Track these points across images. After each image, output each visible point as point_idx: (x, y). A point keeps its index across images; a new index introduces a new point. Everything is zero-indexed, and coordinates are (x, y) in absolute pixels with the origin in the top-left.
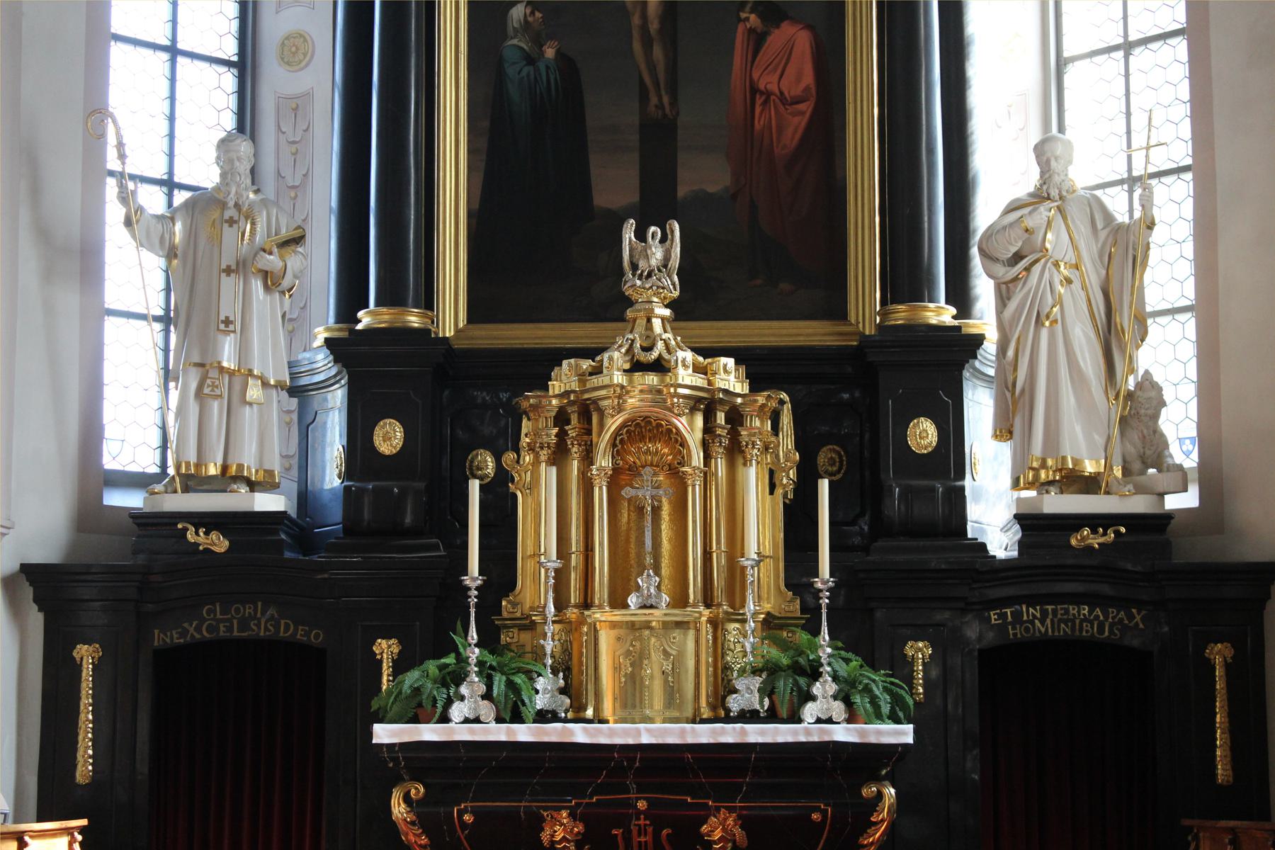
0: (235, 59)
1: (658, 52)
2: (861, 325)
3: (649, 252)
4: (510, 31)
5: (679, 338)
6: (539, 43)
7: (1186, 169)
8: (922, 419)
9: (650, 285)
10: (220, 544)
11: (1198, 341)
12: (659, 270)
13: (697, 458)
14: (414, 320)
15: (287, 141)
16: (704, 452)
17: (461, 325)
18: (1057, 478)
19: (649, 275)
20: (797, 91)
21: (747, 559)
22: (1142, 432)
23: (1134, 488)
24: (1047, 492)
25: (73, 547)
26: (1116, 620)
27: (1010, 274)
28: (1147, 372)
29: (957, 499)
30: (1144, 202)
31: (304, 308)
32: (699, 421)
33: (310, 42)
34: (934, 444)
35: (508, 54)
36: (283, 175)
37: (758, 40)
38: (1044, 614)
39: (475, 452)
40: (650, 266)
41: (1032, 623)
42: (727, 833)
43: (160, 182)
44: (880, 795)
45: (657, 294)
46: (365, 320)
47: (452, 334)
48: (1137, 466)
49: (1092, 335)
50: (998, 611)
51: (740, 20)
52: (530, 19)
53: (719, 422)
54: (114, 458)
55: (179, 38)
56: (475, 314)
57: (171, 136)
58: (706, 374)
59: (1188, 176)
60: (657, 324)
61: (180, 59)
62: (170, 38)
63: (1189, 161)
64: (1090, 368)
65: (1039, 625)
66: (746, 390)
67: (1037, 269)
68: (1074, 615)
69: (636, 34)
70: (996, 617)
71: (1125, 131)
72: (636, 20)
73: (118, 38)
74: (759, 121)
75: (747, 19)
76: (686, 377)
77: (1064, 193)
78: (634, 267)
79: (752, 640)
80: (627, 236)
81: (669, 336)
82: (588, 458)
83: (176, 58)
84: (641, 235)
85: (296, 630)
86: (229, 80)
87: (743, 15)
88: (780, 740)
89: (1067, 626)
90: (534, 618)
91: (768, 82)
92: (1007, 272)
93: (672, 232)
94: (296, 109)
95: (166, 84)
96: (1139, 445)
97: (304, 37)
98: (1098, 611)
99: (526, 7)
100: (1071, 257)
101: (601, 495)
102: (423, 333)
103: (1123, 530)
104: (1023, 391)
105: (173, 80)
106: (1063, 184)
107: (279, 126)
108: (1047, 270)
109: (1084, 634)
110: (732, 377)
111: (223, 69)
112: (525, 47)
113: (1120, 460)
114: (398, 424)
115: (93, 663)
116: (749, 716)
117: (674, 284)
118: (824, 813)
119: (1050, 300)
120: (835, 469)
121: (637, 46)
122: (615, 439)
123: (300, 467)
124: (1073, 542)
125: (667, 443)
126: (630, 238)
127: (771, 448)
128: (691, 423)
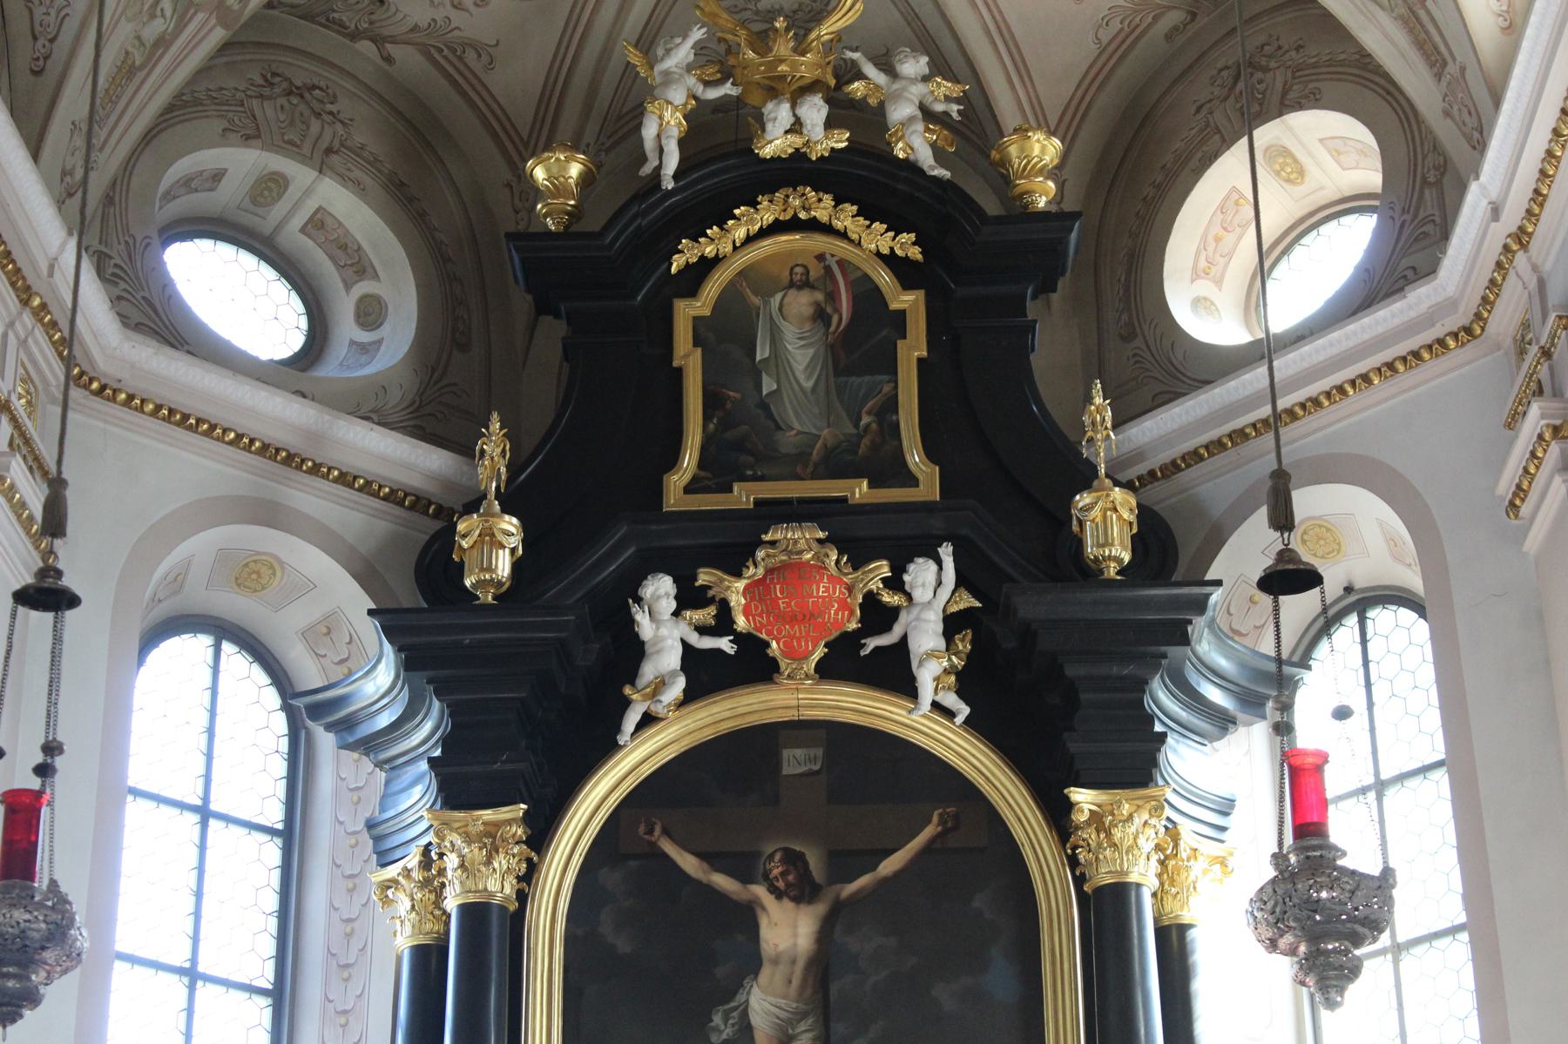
0: (280, 826)
11: (1477, 990)
15: (344, 876)
43: (180, 971)
55: (212, 798)
57: (197, 915)
59: (1464, 936)
61: (212, 822)
62: (201, 795)
63: (1442, 756)
71: (1361, 663)
73: (136, 793)
83: (208, 821)
86: (272, 852)
95: (194, 853)
105: (202, 847)
111: (265, 838)
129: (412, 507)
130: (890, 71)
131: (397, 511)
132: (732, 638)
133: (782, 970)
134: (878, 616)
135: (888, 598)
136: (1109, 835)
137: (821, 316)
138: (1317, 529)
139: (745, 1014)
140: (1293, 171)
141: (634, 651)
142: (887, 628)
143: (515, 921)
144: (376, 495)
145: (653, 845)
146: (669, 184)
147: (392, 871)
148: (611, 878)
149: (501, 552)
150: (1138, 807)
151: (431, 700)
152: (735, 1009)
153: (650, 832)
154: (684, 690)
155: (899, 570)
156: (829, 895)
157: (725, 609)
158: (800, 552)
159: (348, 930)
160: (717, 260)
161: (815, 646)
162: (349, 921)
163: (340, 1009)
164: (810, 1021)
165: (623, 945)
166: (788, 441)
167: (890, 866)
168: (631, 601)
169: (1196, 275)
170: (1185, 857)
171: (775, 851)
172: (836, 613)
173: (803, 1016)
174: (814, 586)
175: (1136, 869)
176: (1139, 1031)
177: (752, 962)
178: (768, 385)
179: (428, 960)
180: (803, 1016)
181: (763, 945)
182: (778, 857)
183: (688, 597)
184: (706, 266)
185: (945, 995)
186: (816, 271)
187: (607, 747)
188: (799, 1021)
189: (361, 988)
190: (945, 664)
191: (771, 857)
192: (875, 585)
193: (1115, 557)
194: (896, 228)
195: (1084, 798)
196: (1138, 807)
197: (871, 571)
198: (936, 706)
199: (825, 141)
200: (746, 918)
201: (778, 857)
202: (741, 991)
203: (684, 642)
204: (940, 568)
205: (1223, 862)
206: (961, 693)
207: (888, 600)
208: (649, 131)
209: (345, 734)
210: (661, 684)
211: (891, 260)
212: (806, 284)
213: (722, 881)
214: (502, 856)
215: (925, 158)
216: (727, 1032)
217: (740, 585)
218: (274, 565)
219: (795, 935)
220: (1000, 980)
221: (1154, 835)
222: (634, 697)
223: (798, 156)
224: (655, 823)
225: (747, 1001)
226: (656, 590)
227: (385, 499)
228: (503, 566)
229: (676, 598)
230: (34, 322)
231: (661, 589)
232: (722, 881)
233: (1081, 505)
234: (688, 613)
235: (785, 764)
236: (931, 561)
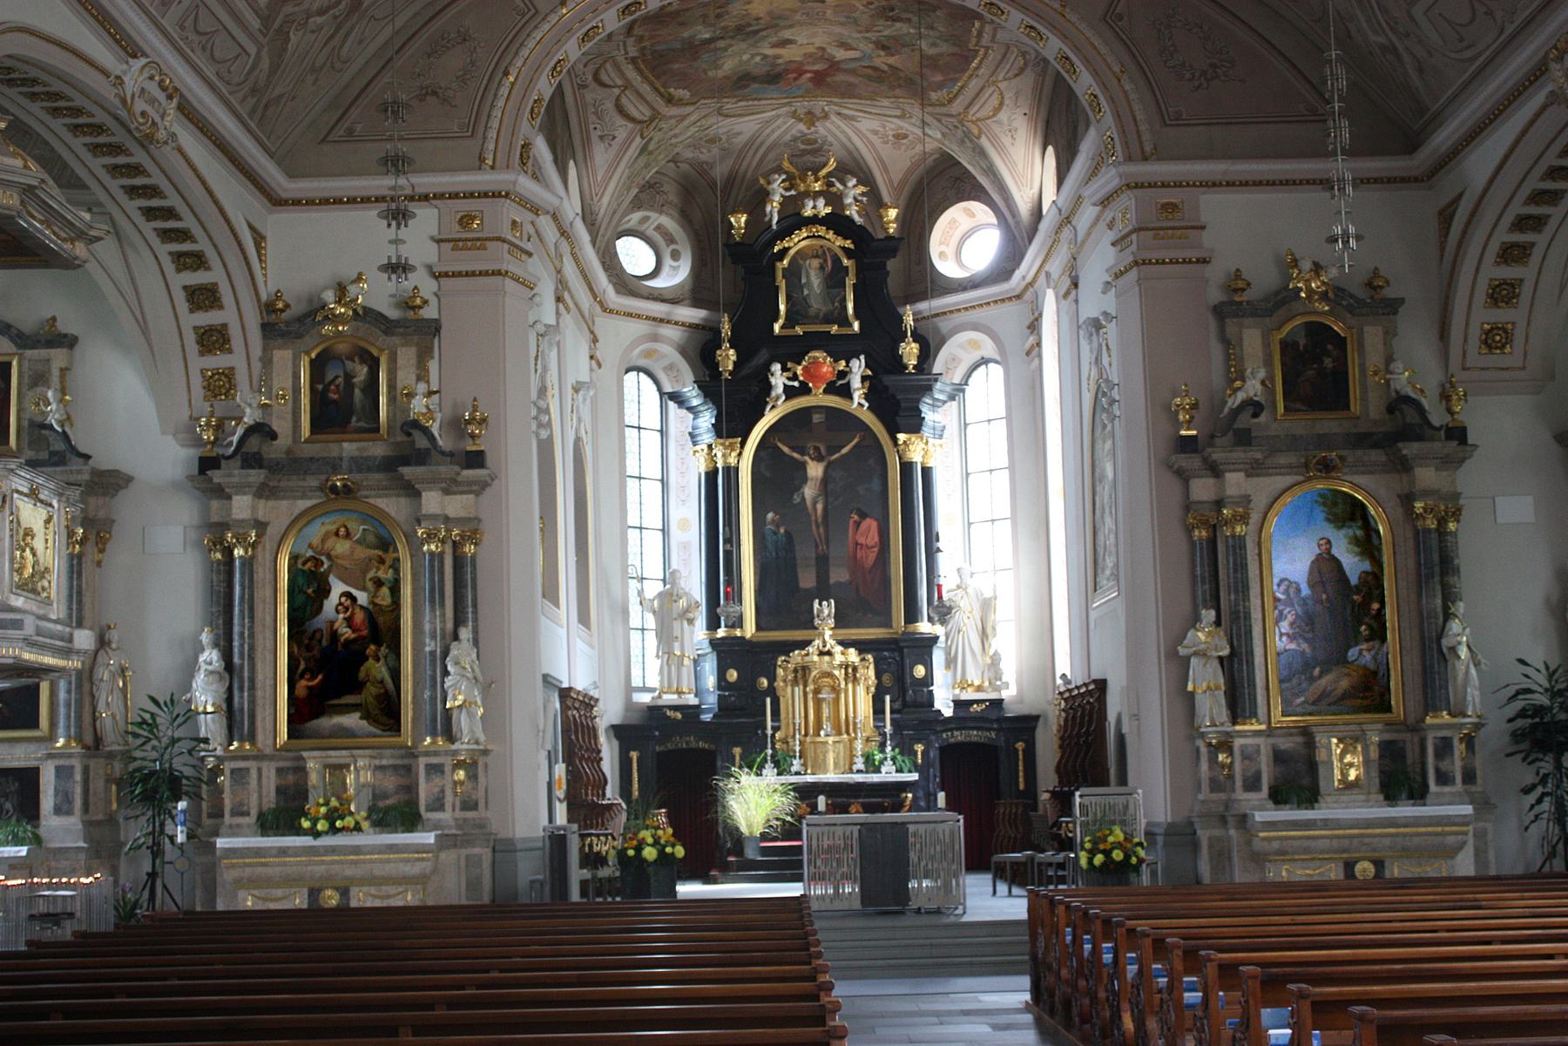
1: (821, 530)
6: (778, 527)
10: (679, 716)
13: (843, 686)
14: (738, 633)
20: (872, 544)
25: (625, 717)
28: (996, 653)
36: (355, 276)
37: (858, 524)
54: (636, 682)
56: (759, 627)
76: (839, 659)
82: (805, 686)
84: (820, 604)
88: (397, 902)
91: (861, 540)
101: (810, 696)
116: (859, 771)
121: (814, 527)
130: (844, 184)
134: (842, 374)
137: (822, 268)
140: (972, 215)
141: (769, 387)
142: (844, 378)
146: (774, 227)
147: (698, 448)
148: (763, 454)
160: (789, 248)
165: (768, 475)
166: (812, 312)
167: (845, 451)
169: (941, 243)
177: (805, 479)
178: (806, 292)
183: (784, 369)
184: (786, 250)
185: (861, 490)
186: (820, 252)
194: (846, 238)
195: (901, 437)
199: (824, 210)
200: (803, 465)
206: (866, 399)
208: (768, 209)
210: (778, 398)
211: (843, 248)
212: (817, 256)
213: (796, 455)
215: (857, 218)
217: (800, 368)
218: (655, 351)
220: (876, 485)
223: (815, 216)
230: (518, 189)
231: (776, 367)
232: (796, 455)
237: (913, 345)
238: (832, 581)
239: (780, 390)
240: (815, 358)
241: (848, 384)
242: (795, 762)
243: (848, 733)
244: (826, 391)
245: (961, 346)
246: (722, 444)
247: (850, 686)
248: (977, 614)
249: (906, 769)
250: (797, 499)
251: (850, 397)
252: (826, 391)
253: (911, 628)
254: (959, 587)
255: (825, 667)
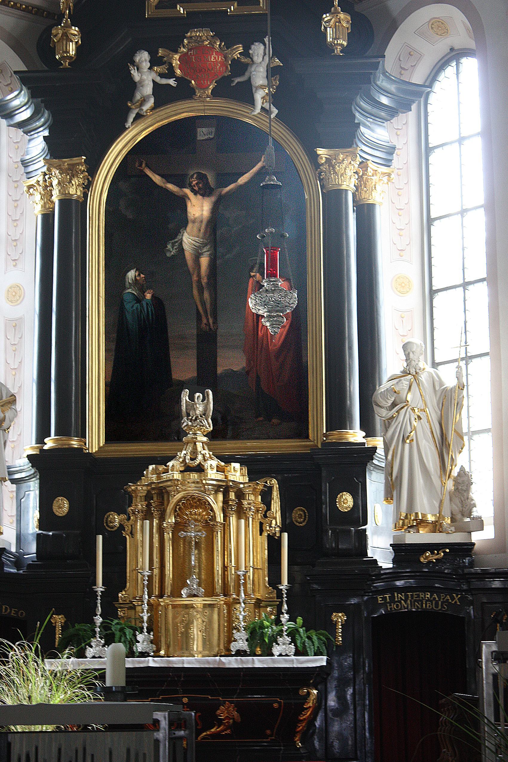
1: (206, 295)
2: (316, 442)
3: (195, 406)
4: (127, 285)
5: (211, 453)
6: (143, 291)
7: (487, 354)
8: (345, 493)
9: (196, 425)
12: (201, 416)
13: (220, 518)
14: (75, 443)
16: (224, 514)
17: (101, 445)
18: (415, 524)
19: (196, 419)
21: (240, 571)
22: (461, 498)
23: (455, 529)
24: (409, 532)
26: (445, 600)
27: (389, 414)
29: (362, 537)
30: (458, 376)
31: (20, 435)
32: (220, 497)
33: (22, 289)
34: (351, 506)
35: (126, 297)
38: (407, 597)
39: (108, 514)
40: (196, 414)
41: (400, 602)
42: (229, 714)
44: (309, 693)
45: (200, 430)
46: (49, 443)
47: (97, 450)
48: (459, 516)
49: (433, 448)
50: (382, 596)
51: (251, 277)
52: (138, 278)
53: (231, 497)
58: (224, 472)
60: (199, 445)
64: (431, 465)
65: (404, 603)
66: (247, 480)
67: (403, 411)
68: (422, 597)
69: (194, 286)
70: (381, 599)
72: (195, 278)
74: (261, 332)
75: (254, 276)
76: (212, 474)
77: (418, 371)
78: (188, 415)
79: (243, 613)
80: (184, 398)
81: (207, 452)
82: (162, 518)
84: (192, 398)
85: (11, 610)
87: (252, 274)
89: (418, 603)
90: (134, 603)
92: (389, 413)
93: (208, 395)
94: (15, 327)
96: (460, 505)
97: (19, 287)
98: (435, 596)
99: (135, 271)
100: (421, 405)
101: (168, 535)
102: (80, 450)
103: (448, 550)
104: (397, 477)
106: (417, 366)
107: (6, 336)
108: (408, 413)
109: (428, 608)
110: (238, 473)
112: (135, 293)
113: (449, 514)
114: (65, 499)
115: (61, 626)
116: (240, 653)
117: (209, 424)
118: (280, 703)
119: (409, 430)
120: (302, 520)
121: (195, 292)
122: (176, 508)
123: (17, 520)
124: (422, 560)
125: (205, 509)
126: (186, 400)
127: (261, 511)
128: (216, 499)
129: (36, 13)
131: (30, 16)
132: (174, 79)
133: (197, 224)
135: (244, 60)
136: (334, 168)
138: (438, 23)
139: (181, 244)
143: (82, 205)
144: (19, 9)
145: (142, 171)
149: (71, 43)
150: (347, 156)
151: (44, 111)
152: (177, 242)
153: (140, 165)
154: (154, 103)
155: (247, 48)
156: (217, 193)
157: (171, 69)
158: (203, 41)
159: (16, 205)
161: (211, 83)
162: (16, 201)
163: (13, 239)
164: (208, 247)
168: (129, 64)
170: (370, 174)
171: (194, 174)
172: (220, 68)
173: (205, 245)
174: (209, 57)
175: (345, 183)
176: (344, 252)
179: (47, 219)
180: (205, 245)
181: (189, 215)
182: (195, 176)
183: (155, 62)
187: (122, 129)
188: (203, 247)
189: (22, 230)
190: (267, 91)
191: (192, 176)
192: (236, 55)
193: (340, 44)
196: (347, 156)
197: (234, 49)
198: (262, 108)
201: (195, 176)
202: (179, 234)
203: (153, 81)
204: (265, 48)
205: (389, 175)
207: (243, 61)
209: (9, 120)
210: (144, 101)
213: (171, 187)
214: (76, 178)
216: (173, 252)
217: (177, 56)
219: (203, 210)
221: (353, 168)
222: (133, 107)
224: (142, 162)
225: (182, 238)
226: (141, 58)
227: (24, 10)
228: (72, 49)
229: (150, 62)
232: (171, 187)
233: (326, 19)
234: (155, 68)
235: (198, 134)
236: (261, 44)
237: (342, 16)
238: (220, 370)
239: (148, 89)
240: (199, 40)
241: (249, 82)
242: (140, 637)
243: (226, 594)
244: (215, 94)
245: (420, 33)
246: (59, 167)
247: (233, 520)
248: (433, 414)
249: (311, 649)
250: (171, 250)
251: (251, 102)
252: (215, 94)
253: (334, 436)
254: (406, 373)
255: (192, 489)
